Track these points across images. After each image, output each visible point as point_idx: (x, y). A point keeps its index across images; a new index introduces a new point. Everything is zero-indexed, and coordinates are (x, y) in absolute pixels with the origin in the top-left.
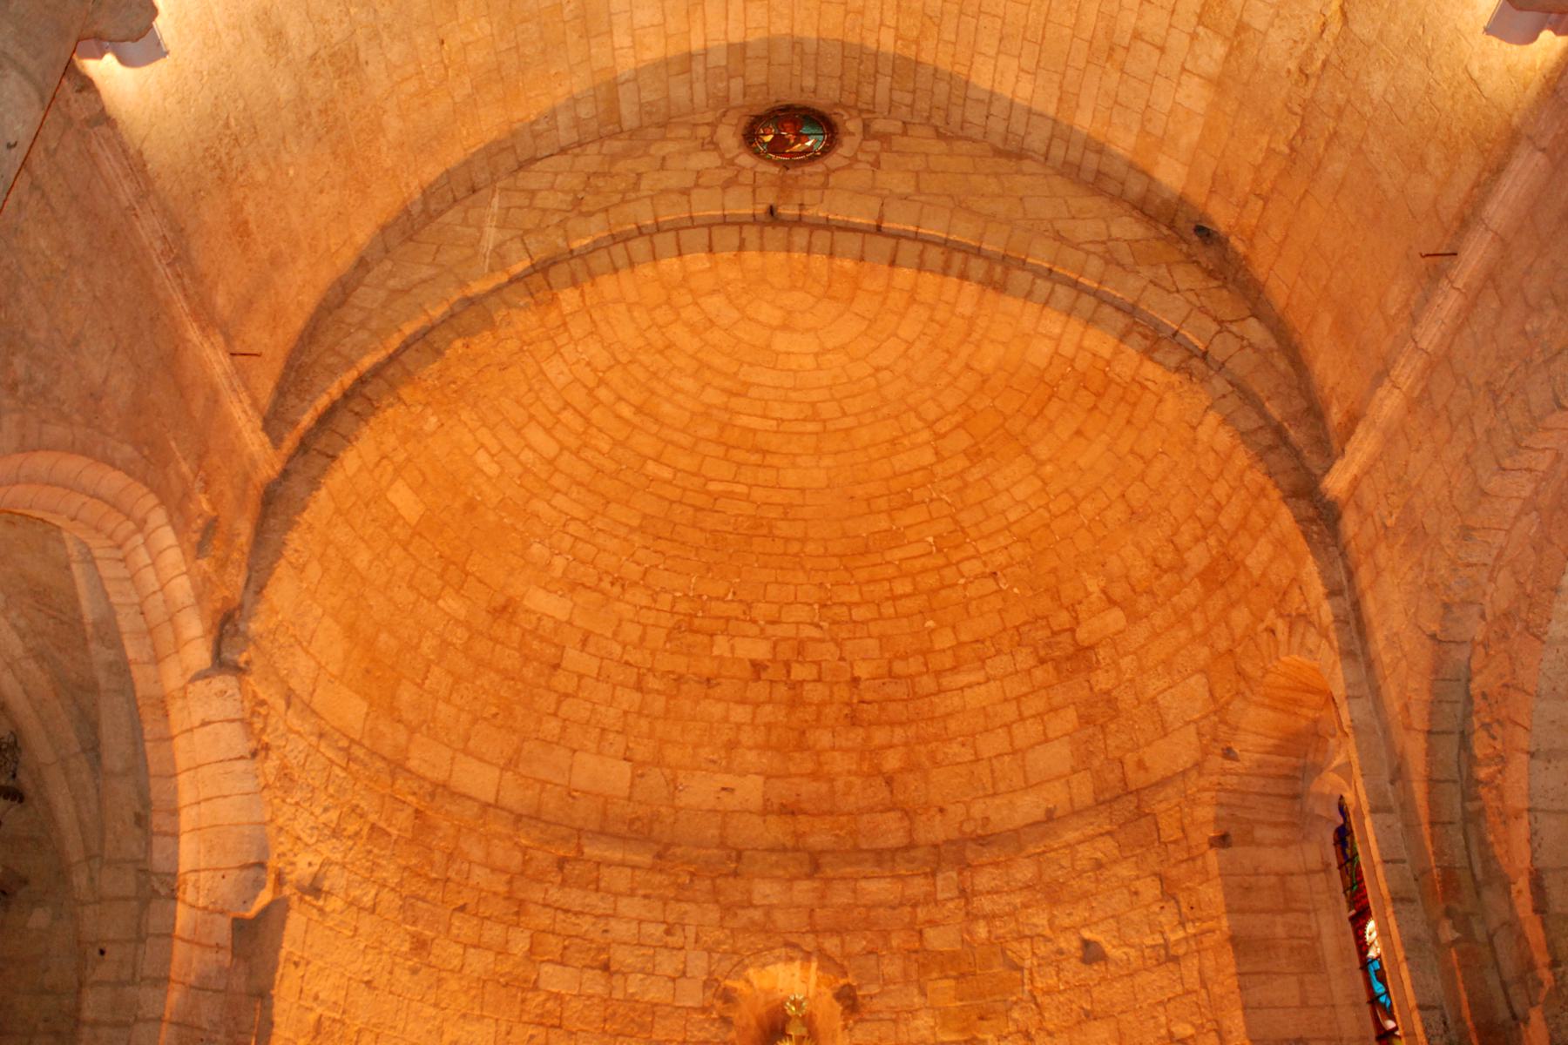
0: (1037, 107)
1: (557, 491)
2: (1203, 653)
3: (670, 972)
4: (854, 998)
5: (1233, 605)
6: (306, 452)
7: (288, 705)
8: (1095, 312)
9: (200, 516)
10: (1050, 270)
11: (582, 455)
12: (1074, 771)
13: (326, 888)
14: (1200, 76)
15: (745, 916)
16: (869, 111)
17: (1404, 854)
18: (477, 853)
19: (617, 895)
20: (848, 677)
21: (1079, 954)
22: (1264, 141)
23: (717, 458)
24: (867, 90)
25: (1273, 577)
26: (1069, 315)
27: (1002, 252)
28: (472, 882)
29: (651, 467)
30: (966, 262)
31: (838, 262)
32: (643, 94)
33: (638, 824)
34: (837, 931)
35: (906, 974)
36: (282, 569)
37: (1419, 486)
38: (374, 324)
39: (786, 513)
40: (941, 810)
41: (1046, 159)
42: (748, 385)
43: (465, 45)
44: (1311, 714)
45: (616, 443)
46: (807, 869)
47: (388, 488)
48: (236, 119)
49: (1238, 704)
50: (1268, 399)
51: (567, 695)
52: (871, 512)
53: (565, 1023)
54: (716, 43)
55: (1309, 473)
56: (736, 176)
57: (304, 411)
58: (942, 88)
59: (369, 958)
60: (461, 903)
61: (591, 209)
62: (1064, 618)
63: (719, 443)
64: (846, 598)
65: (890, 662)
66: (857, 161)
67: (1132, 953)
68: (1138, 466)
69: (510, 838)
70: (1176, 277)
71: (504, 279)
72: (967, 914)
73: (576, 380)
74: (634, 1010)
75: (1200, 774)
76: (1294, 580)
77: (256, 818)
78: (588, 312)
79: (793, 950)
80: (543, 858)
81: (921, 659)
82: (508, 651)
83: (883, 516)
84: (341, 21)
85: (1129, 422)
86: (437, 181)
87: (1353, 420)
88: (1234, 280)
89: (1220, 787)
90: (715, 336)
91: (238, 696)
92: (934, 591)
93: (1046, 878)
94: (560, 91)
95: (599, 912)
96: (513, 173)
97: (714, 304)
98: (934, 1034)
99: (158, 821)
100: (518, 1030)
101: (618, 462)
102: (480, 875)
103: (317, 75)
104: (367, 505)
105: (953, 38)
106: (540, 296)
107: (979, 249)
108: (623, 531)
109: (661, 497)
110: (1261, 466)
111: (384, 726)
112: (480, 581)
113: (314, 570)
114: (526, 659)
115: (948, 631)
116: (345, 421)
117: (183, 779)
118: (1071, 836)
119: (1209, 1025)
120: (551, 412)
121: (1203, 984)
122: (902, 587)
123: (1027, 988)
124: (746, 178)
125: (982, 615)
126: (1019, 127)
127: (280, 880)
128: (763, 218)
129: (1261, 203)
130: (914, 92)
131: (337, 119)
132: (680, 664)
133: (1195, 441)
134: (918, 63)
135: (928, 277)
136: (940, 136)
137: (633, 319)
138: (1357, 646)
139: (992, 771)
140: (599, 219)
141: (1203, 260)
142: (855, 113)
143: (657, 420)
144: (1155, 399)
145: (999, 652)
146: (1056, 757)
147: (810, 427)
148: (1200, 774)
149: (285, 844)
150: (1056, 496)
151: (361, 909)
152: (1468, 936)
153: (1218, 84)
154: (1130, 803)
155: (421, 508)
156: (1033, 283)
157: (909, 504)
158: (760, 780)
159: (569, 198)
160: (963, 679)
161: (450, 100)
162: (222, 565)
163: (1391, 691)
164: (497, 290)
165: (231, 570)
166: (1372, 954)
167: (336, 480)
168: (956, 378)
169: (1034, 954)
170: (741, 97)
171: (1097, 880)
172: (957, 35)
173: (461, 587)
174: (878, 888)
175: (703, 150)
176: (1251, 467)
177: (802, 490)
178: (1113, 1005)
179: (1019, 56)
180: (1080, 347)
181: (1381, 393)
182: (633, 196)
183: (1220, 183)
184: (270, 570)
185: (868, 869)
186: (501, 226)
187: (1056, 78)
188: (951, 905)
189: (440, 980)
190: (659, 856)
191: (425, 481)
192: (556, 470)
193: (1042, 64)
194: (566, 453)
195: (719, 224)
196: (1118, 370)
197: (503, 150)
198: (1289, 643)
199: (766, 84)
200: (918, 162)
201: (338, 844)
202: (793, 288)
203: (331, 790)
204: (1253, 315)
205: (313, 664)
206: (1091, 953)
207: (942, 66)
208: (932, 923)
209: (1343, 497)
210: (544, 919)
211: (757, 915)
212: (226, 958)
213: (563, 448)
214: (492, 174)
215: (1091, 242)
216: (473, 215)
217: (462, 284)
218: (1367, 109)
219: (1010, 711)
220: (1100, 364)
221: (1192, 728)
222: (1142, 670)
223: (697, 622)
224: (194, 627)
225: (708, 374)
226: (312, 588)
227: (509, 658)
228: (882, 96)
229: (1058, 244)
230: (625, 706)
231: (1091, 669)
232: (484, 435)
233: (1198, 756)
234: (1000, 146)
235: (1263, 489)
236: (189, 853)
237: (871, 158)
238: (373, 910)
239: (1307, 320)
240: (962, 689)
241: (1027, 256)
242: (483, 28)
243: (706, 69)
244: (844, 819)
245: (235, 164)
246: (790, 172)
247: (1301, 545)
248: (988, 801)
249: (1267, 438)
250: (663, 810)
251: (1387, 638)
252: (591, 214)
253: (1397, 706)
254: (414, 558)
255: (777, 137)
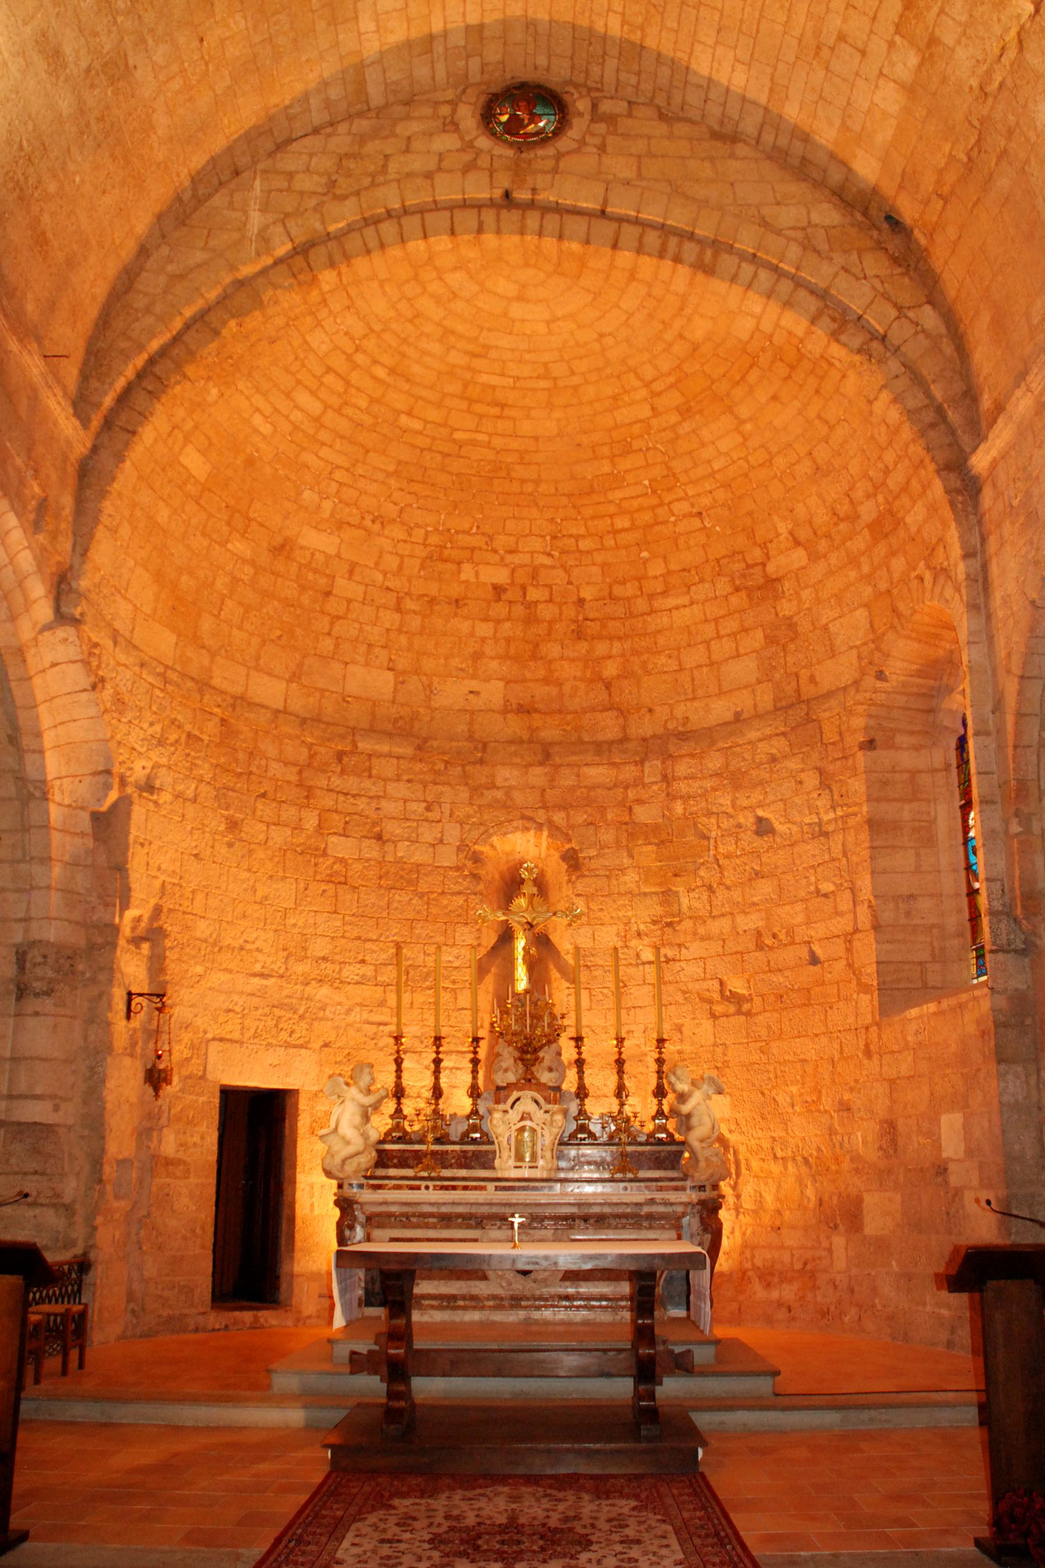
0: (750, 95)
1: (323, 444)
2: (867, 591)
3: (430, 840)
4: (577, 859)
5: (893, 554)
6: (109, 429)
7: (115, 643)
8: (791, 295)
9: (33, 498)
10: (754, 255)
11: (344, 412)
12: (759, 682)
13: (157, 785)
14: (895, 81)
15: (489, 795)
16: (598, 90)
17: (994, 768)
18: (272, 751)
19: (386, 780)
20: (575, 598)
21: (754, 828)
22: (947, 148)
23: (461, 410)
24: (596, 70)
25: (925, 535)
26: (769, 297)
27: (712, 237)
28: (270, 774)
29: (404, 419)
30: (680, 245)
31: (566, 244)
32: (388, 75)
33: (401, 723)
34: (564, 807)
35: (618, 841)
36: (100, 533)
37: (1037, 478)
38: (158, 309)
39: (522, 458)
40: (650, 710)
41: (758, 143)
42: (487, 347)
43: (222, 41)
44: (948, 646)
45: (373, 401)
46: (540, 757)
47: (180, 453)
48: (28, 141)
49: (890, 636)
50: (934, 381)
51: (339, 618)
52: (596, 458)
53: (350, 880)
54: (454, 25)
55: (962, 451)
56: (475, 159)
57: (106, 393)
58: (665, 71)
59: (195, 837)
60: (262, 791)
61: (343, 192)
62: (757, 554)
63: (462, 397)
64: (574, 531)
65: (611, 587)
66: (585, 144)
67: (795, 829)
68: (824, 430)
69: (297, 737)
70: (865, 263)
71: (270, 261)
72: (668, 795)
73: (336, 348)
74: (403, 869)
75: (857, 691)
76: (940, 539)
77: (101, 736)
78: (345, 289)
79: (528, 822)
80: (325, 753)
81: (637, 584)
82: (287, 583)
83: (606, 462)
84: (110, 31)
85: (817, 392)
86: (203, 168)
87: (999, 408)
88: (916, 269)
89: (872, 703)
90: (459, 306)
91: (77, 643)
92: (648, 527)
93: (732, 768)
94: (312, 76)
95: (372, 794)
96: (271, 154)
97: (456, 279)
98: (639, 887)
99: (26, 741)
100: (313, 886)
101: (376, 417)
102: (276, 769)
103: (92, 86)
104: (164, 470)
105: (675, 25)
106: (301, 277)
107: (693, 233)
108: (381, 476)
109: (413, 446)
110: (922, 442)
111: (190, 652)
112: (262, 525)
113: (125, 531)
114: (303, 588)
115: (660, 561)
116: (140, 399)
117: (42, 709)
118: (753, 735)
119: (846, 885)
120: (314, 376)
121: (845, 854)
122: (622, 523)
123: (712, 852)
124: (484, 161)
125: (689, 548)
126: (733, 112)
127: (123, 782)
128: (499, 201)
129: (941, 202)
130: (639, 73)
131: (113, 124)
132: (433, 588)
133: (871, 413)
134: (642, 47)
135: (645, 260)
136: (662, 117)
137: (385, 293)
138: (981, 601)
139: (693, 679)
140: (351, 203)
141: (890, 247)
142: (584, 91)
143: (408, 380)
144: (839, 376)
145: (702, 581)
146: (745, 669)
147: (543, 384)
148: (857, 691)
149: (123, 754)
150: (755, 450)
151: (186, 800)
152: (1028, 830)
153: (910, 90)
154: (801, 711)
155: (208, 468)
156: (739, 267)
157: (628, 451)
158: (501, 684)
159: (324, 180)
160: (671, 602)
161: (211, 94)
162: (54, 536)
163: (1000, 641)
164: (264, 272)
165: (61, 539)
166: (972, 834)
167: (137, 452)
168: (671, 345)
169: (719, 827)
170: (479, 75)
171: (771, 771)
172: (679, 23)
173: (246, 532)
174: (597, 773)
175: (444, 131)
176: (914, 441)
177: (536, 439)
178: (776, 867)
179: (736, 47)
180: (777, 325)
181: (1018, 393)
182: (382, 179)
183: (907, 180)
184: (91, 536)
185: (589, 758)
186: (264, 210)
187: (769, 70)
188: (655, 787)
189: (250, 851)
190: (419, 748)
191: (211, 444)
192: (322, 426)
193: (756, 56)
194: (330, 412)
195: (459, 207)
196: (809, 347)
197: (260, 135)
198: (932, 591)
199: (503, 62)
200: (639, 146)
201: (163, 750)
202: (527, 265)
203: (154, 708)
204: (928, 302)
205: (130, 607)
206: (763, 828)
207: (664, 51)
208: (640, 801)
209: (985, 474)
210: (329, 801)
211: (499, 794)
212: (90, 843)
213: (327, 407)
214: (253, 157)
215: (792, 228)
216: (237, 197)
217: (232, 268)
218: (1032, 134)
219: (709, 630)
220: (795, 341)
221: (854, 652)
222: (818, 601)
223: (446, 553)
224: (38, 589)
225: (452, 339)
226: (125, 545)
227: (290, 590)
228: (609, 76)
229: (763, 229)
230: (387, 625)
231: (776, 598)
232: (259, 401)
233: (857, 675)
234: (717, 128)
235: (922, 461)
236: (53, 765)
237: (597, 141)
238: (194, 800)
239: (971, 313)
240: (670, 610)
241: (735, 241)
242: (238, 23)
243: (446, 49)
244: (569, 717)
245: (30, 182)
246: (524, 155)
247: (947, 512)
248: (689, 704)
249: (929, 416)
250: (421, 710)
251: (1003, 598)
252: (344, 198)
253: (1003, 654)
254: (205, 509)
255: (513, 117)
